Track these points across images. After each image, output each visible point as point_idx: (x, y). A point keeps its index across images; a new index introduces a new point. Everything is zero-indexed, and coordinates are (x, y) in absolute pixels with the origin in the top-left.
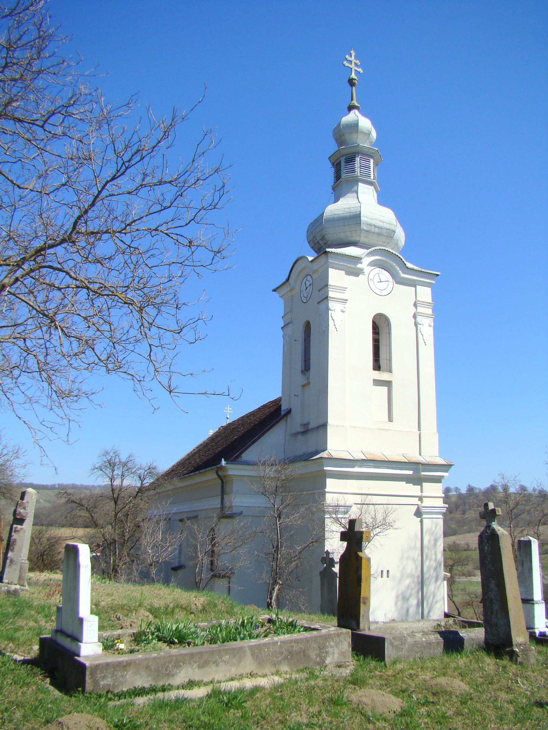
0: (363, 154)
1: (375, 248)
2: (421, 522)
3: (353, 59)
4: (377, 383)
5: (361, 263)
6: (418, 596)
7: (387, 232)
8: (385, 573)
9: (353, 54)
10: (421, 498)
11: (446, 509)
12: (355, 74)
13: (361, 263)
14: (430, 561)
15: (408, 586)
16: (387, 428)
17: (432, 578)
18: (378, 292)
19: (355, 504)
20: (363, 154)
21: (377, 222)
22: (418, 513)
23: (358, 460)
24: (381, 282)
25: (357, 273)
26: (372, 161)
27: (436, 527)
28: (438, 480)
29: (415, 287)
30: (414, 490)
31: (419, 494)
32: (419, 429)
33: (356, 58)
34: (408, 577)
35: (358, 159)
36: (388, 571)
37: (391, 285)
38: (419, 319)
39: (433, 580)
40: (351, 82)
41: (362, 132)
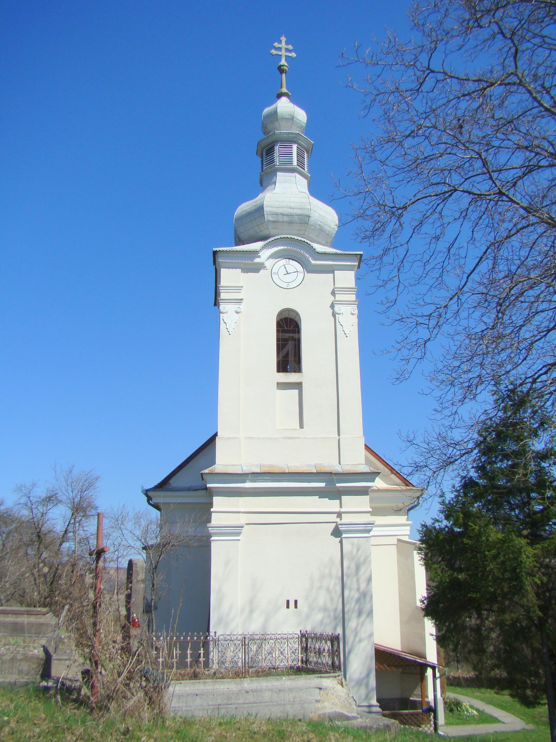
0: (283, 141)
1: (275, 238)
2: (341, 542)
3: (283, 44)
4: (282, 386)
5: (259, 257)
7: (299, 218)
8: (292, 604)
9: (283, 39)
10: (339, 515)
11: (408, 528)
12: (286, 60)
13: (259, 257)
15: (322, 622)
19: (247, 524)
20: (283, 141)
22: (337, 533)
23: (249, 474)
24: (288, 274)
25: (257, 268)
26: (295, 147)
27: (358, 550)
28: (364, 492)
29: (333, 272)
30: (332, 505)
31: (337, 509)
32: (339, 435)
33: (287, 43)
35: (277, 148)
36: (296, 602)
37: (301, 276)
38: (336, 308)
39: (355, 614)
40: (281, 70)
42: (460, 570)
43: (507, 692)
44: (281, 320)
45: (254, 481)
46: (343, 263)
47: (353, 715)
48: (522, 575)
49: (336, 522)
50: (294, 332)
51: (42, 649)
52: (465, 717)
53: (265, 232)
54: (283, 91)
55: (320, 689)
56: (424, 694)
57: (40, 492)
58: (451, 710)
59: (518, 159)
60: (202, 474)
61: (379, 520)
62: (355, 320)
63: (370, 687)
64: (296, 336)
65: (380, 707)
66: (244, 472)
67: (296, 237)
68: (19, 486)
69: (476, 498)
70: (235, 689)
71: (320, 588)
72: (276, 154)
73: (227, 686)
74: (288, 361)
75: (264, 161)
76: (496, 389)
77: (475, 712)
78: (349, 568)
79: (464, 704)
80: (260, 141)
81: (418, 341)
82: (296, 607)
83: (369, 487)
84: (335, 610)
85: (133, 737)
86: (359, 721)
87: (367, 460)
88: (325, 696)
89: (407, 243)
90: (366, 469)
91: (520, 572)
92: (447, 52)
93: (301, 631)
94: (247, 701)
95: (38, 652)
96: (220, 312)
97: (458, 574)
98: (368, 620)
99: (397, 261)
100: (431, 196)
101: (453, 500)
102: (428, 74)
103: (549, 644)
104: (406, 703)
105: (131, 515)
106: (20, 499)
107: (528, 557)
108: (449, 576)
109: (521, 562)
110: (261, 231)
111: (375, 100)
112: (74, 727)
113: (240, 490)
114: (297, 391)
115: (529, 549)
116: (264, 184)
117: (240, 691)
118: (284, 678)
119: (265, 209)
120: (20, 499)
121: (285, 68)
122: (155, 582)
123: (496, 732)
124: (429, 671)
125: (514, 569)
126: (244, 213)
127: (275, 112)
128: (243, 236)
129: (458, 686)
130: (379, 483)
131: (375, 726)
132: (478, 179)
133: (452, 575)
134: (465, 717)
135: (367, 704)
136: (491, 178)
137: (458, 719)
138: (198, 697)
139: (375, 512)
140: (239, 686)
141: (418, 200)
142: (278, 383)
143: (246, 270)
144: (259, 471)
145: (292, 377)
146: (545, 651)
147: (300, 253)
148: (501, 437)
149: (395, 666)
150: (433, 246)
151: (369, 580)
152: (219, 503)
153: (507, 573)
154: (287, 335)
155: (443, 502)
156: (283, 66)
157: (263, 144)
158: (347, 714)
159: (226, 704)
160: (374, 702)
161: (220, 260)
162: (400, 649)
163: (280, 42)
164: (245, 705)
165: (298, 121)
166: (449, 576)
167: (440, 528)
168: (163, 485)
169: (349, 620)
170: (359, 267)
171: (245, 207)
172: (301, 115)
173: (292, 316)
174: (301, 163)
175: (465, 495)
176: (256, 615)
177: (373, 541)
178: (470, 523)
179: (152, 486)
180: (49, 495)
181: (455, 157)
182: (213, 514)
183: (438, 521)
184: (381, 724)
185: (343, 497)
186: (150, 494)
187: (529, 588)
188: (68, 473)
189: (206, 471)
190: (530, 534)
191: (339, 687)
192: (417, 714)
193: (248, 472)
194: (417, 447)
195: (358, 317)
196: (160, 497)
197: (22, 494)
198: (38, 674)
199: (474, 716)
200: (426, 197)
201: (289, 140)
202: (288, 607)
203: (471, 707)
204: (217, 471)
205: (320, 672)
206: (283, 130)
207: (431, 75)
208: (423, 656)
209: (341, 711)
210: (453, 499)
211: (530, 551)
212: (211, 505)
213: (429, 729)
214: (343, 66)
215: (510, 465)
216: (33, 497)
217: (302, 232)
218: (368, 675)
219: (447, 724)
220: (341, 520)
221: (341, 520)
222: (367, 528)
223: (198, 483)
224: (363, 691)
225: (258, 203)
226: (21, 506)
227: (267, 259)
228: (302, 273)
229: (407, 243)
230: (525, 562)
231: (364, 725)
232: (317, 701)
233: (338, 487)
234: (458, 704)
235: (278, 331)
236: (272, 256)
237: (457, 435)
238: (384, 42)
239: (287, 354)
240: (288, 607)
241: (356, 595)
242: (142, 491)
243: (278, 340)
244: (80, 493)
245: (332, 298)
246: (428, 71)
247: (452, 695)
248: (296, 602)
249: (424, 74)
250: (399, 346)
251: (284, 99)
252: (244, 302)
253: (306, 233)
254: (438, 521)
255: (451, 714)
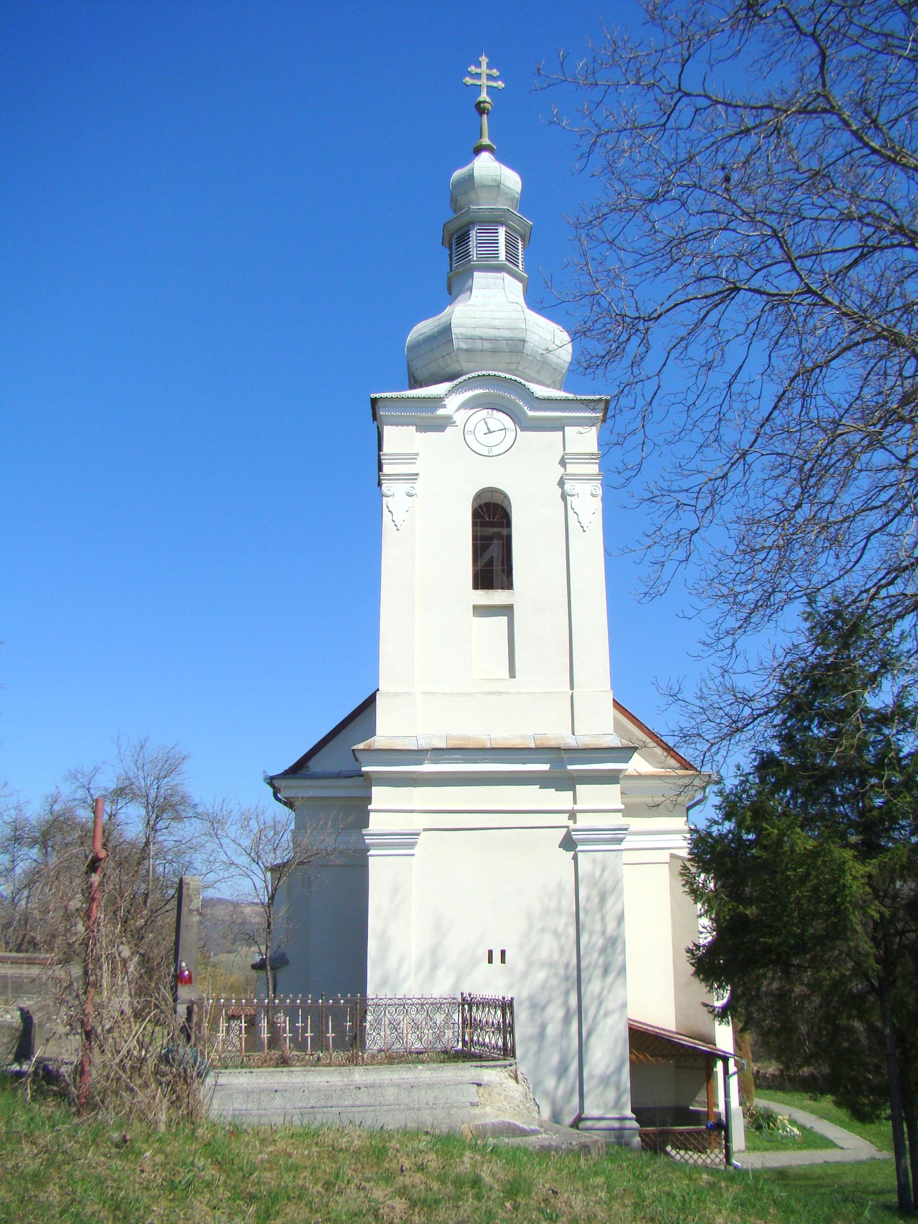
0: (482, 222)
1: (469, 376)
2: (575, 858)
3: (484, 66)
4: (481, 611)
5: (444, 406)
6: (566, 1003)
8: (497, 956)
9: (484, 60)
10: (572, 815)
13: (444, 406)
14: (591, 934)
16: (501, 690)
17: (596, 966)
18: (484, 451)
19: (425, 830)
20: (482, 222)
21: (486, 330)
22: (568, 843)
23: (427, 750)
24: (490, 432)
25: (441, 425)
26: (502, 231)
27: (603, 870)
28: (611, 778)
29: (562, 429)
30: (561, 799)
31: (569, 806)
32: (572, 687)
33: (489, 66)
34: (543, 965)
35: (473, 234)
36: (503, 953)
37: (511, 435)
38: (568, 487)
39: (598, 972)
40: (480, 109)
41: (483, 186)
42: (749, 902)
43: (829, 1098)
44: (480, 507)
45: (436, 762)
46: (574, 414)
47: (532, 1127)
48: (846, 908)
49: (568, 827)
50: (500, 525)
51: (19, 1013)
52: (779, 1138)
53: (455, 368)
54: (484, 143)
55: (479, 1085)
56: (711, 1102)
57: (107, 781)
58: (759, 1128)
59: (850, 236)
60: (353, 750)
61: (637, 824)
62: (597, 504)
63: (622, 1087)
64: (504, 531)
65: (637, 1120)
66: (420, 748)
67: (502, 375)
68: (73, 771)
69: (779, 786)
70: (339, 1083)
71: (543, 930)
72: (473, 243)
73: (327, 1078)
74: (492, 571)
75: (454, 255)
76: (810, 610)
77: (795, 1130)
78: (588, 898)
79: (780, 1117)
80: (448, 223)
81: (681, 533)
82: (503, 961)
83: (620, 771)
84: (567, 966)
85: (131, 1150)
86: (544, 1138)
87: (617, 724)
88: (486, 1096)
89: (658, 375)
90: (614, 741)
91: (843, 903)
92: (713, 62)
93: (462, 994)
94: (358, 1103)
95: (12, 1018)
96: (383, 496)
97: (745, 908)
98: (619, 981)
99: (641, 403)
100: (696, 298)
101: (736, 788)
102: (680, 98)
103: (895, 1021)
104: (686, 1116)
105: (236, 815)
106: (75, 792)
107: (855, 878)
108: (729, 910)
109: (844, 886)
110: (448, 366)
111: (595, 143)
112: (37, 1133)
113: (415, 776)
114: (506, 618)
115: (858, 866)
116: (454, 291)
117: (347, 1085)
118: (420, 1067)
119: (454, 330)
120: (75, 792)
121: (487, 105)
122: (271, 920)
123: (826, 1162)
124: (720, 1064)
125: (832, 899)
126: (421, 337)
127: (470, 177)
128: (421, 375)
129: (780, 1090)
130: (638, 764)
131: (563, 1146)
132: (775, 270)
133: (734, 910)
134: (779, 1138)
135: (617, 1116)
136: (794, 268)
137: (769, 1141)
138: (278, 1095)
139: (629, 811)
140: (346, 1079)
141: (676, 305)
142: (474, 607)
143: (426, 426)
144: (444, 746)
145: (497, 597)
146: (887, 1031)
147: (509, 400)
148: (817, 687)
149: (663, 1056)
150: (701, 379)
151: (620, 919)
152: (381, 796)
153: (821, 905)
154: (491, 531)
155: (720, 792)
156: (484, 102)
157: (454, 227)
158: (521, 1125)
159: (324, 1107)
160: (628, 1113)
161: (382, 413)
162: (674, 1029)
163: (478, 65)
164: (354, 1109)
165: (507, 190)
166: (729, 910)
167: (720, 835)
168: (298, 769)
169: (589, 980)
170: (604, 420)
171: (423, 328)
172: (512, 180)
173: (497, 500)
174: (512, 256)
175: (763, 780)
176: (441, 972)
177: (627, 857)
178: (764, 825)
179: (280, 770)
180: (120, 786)
181: (732, 234)
182: (371, 814)
183: (716, 822)
184: (574, 1143)
185: (579, 788)
186: (277, 783)
187: (859, 928)
188: (138, 749)
189: (361, 746)
190: (863, 843)
191: (512, 1082)
192: (699, 1133)
193: (426, 747)
194: (683, 704)
195: (603, 500)
196: (297, 789)
197: (77, 784)
198: (10, 1052)
199: (793, 1137)
200: (688, 301)
201: (493, 220)
202: (490, 961)
203: (793, 1122)
204: (378, 746)
205: (480, 1057)
206: (484, 204)
207: (685, 100)
208: (711, 1041)
209: (512, 1121)
210: (736, 787)
211: (860, 869)
212: (369, 799)
213: (717, 1156)
214: (541, 89)
215: (832, 733)
216: (95, 788)
217: (513, 366)
218: (619, 1070)
219: (751, 1147)
220: (575, 822)
221: (575, 822)
222: (616, 836)
223: (346, 765)
224: (611, 1095)
225: (443, 320)
226: (76, 802)
227: (457, 410)
228: (512, 430)
229: (658, 375)
230: (851, 887)
231: (546, 1143)
232: (473, 1105)
233: (570, 770)
234: (770, 1117)
235: (474, 524)
236: (466, 405)
237: (750, 684)
238: (605, 48)
239: (491, 560)
240: (490, 961)
241: (600, 942)
242: (265, 780)
243: (475, 538)
244: (156, 782)
245: (561, 470)
246: (679, 94)
247: (761, 1102)
248: (503, 953)
249: (672, 98)
250: (649, 541)
251: (485, 156)
252: (420, 478)
253: (520, 368)
254: (716, 822)
255: (757, 1133)
